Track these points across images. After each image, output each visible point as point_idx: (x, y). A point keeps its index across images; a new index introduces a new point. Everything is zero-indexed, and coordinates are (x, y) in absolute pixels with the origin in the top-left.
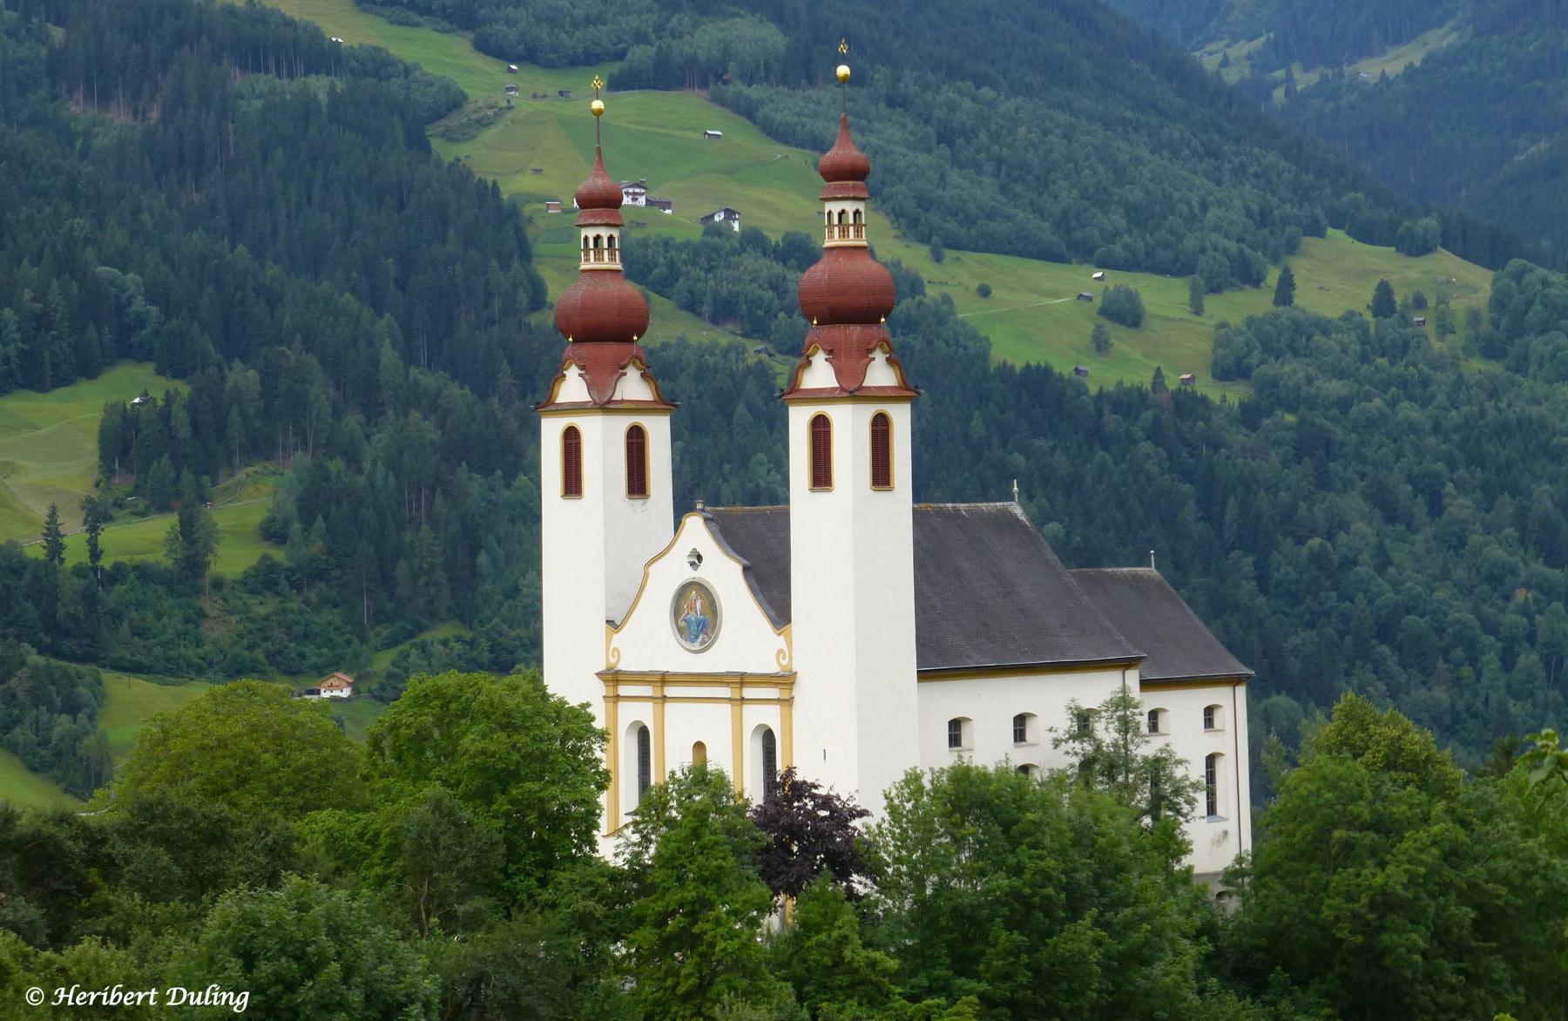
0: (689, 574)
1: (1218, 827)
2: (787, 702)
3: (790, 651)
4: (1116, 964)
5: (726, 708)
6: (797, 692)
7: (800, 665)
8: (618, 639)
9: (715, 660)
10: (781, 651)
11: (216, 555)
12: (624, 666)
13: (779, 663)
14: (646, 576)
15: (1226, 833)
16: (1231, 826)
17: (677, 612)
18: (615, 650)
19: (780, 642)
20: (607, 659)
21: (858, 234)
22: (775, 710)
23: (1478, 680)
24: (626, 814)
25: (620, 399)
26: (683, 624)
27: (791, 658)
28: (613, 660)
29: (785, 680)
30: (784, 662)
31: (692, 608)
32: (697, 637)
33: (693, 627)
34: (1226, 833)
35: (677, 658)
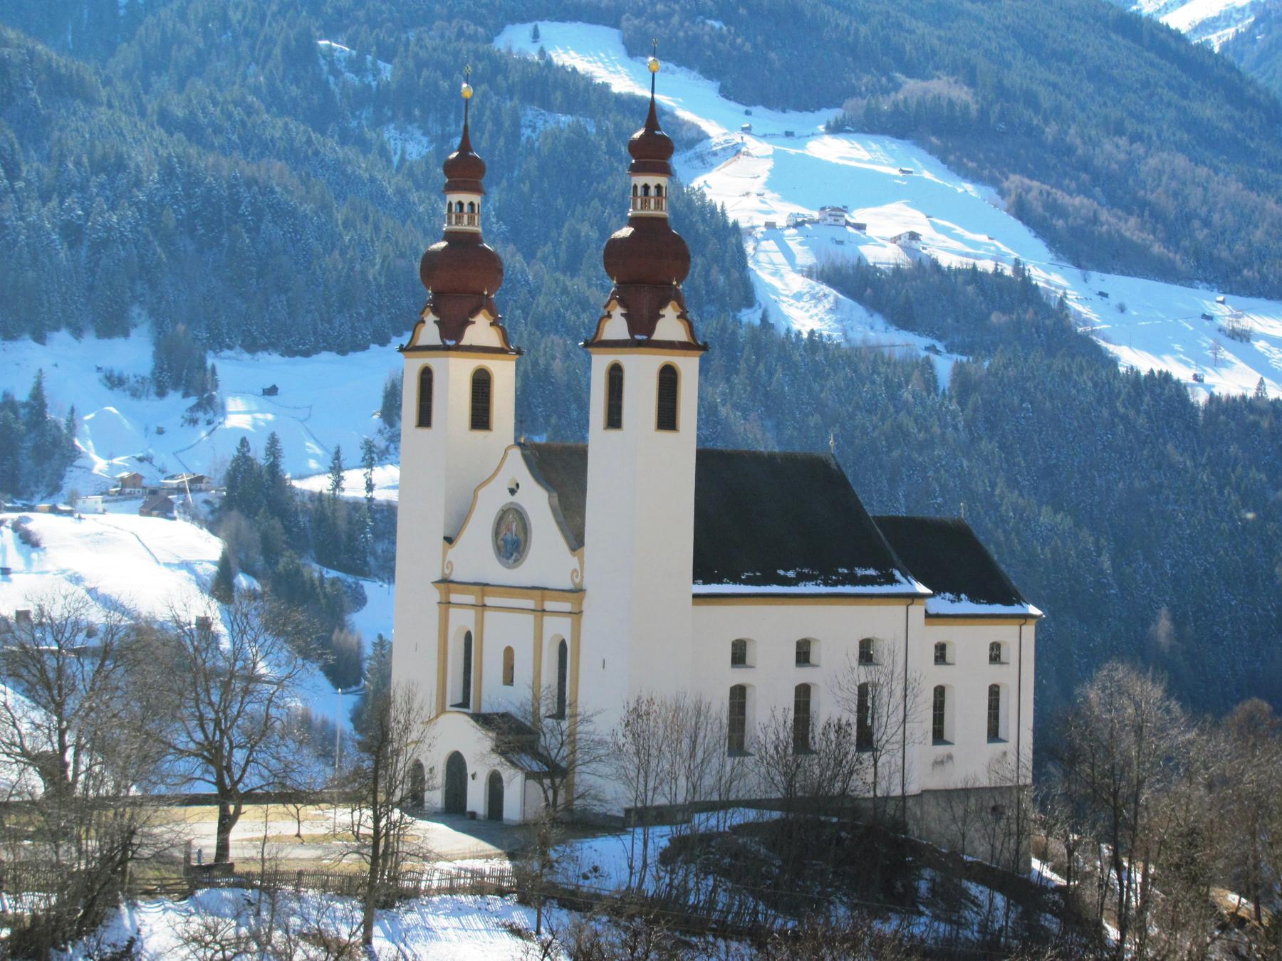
0: (509, 498)
1: (998, 747)
2: (577, 614)
3: (582, 569)
4: (777, 871)
5: (530, 618)
6: (586, 605)
7: (586, 585)
8: (455, 552)
9: (524, 574)
10: (575, 570)
11: (619, 885)
12: (454, 577)
13: (572, 580)
14: (475, 497)
15: (1005, 754)
16: (1010, 746)
17: (497, 533)
18: (450, 563)
19: (573, 562)
20: (443, 570)
21: (658, 205)
22: (567, 621)
23: (307, 920)
24: (452, 706)
25: (468, 344)
26: (501, 543)
27: (582, 577)
28: (447, 572)
29: (578, 591)
30: (577, 581)
31: (509, 530)
32: (512, 555)
33: (509, 546)
34: (1005, 754)
35: (497, 572)
